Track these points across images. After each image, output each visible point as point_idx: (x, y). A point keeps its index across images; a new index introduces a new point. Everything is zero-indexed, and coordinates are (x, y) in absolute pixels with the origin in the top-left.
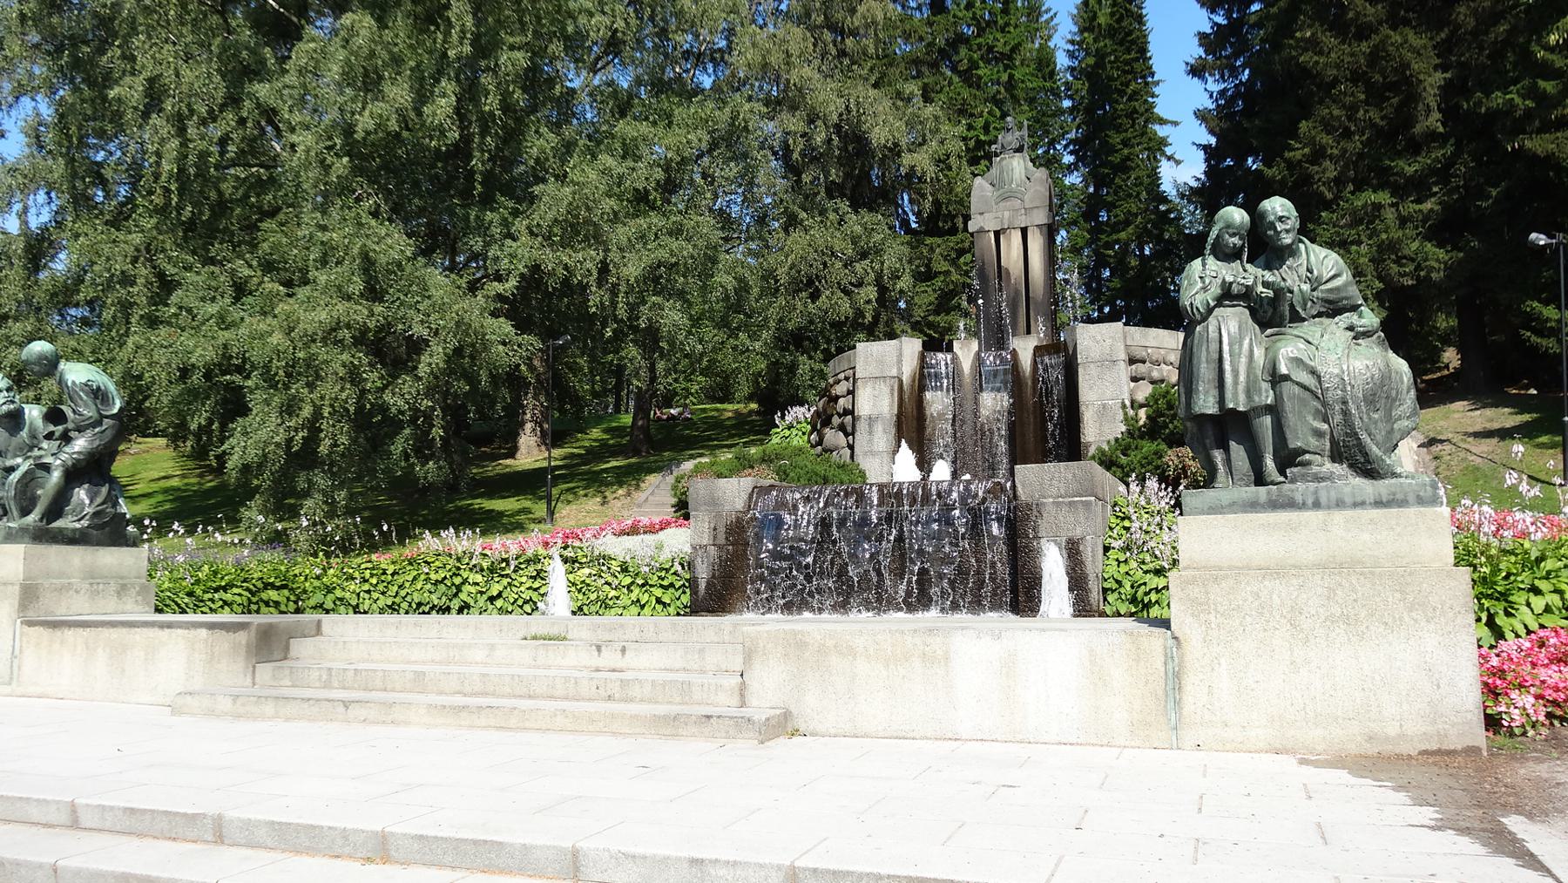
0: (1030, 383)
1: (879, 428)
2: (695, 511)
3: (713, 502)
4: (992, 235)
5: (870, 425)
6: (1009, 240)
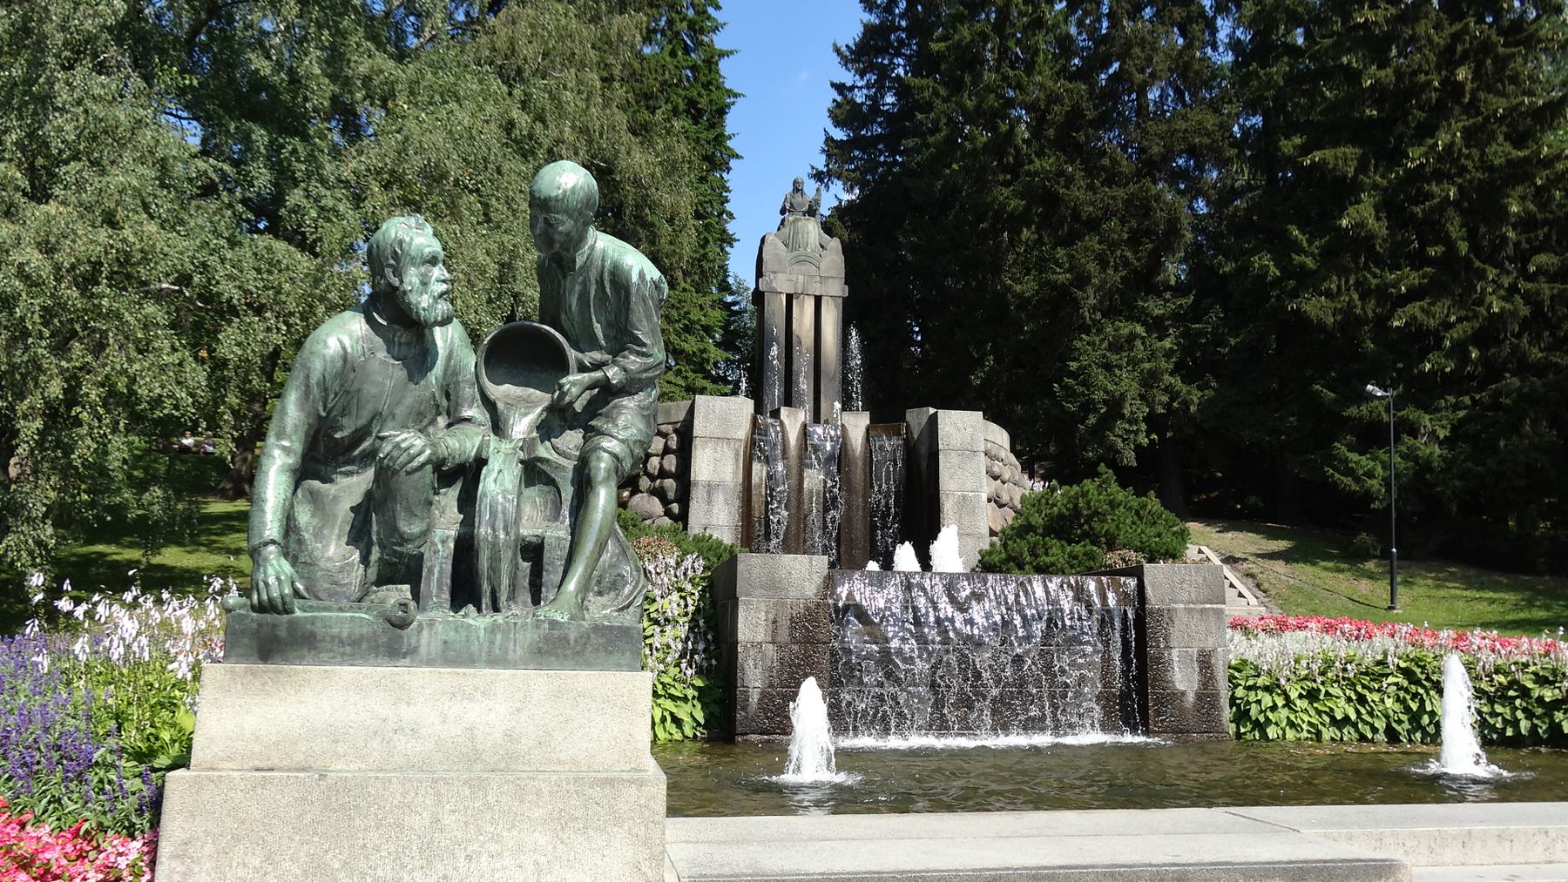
0: (860, 463)
1: (719, 499)
2: (747, 595)
3: (773, 586)
4: (784, 297)
5: (709, 493)
6: (802, 306)
